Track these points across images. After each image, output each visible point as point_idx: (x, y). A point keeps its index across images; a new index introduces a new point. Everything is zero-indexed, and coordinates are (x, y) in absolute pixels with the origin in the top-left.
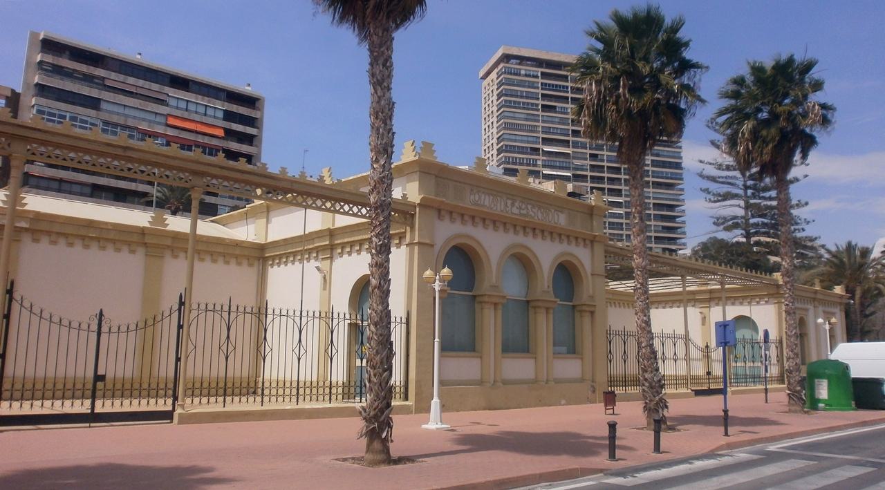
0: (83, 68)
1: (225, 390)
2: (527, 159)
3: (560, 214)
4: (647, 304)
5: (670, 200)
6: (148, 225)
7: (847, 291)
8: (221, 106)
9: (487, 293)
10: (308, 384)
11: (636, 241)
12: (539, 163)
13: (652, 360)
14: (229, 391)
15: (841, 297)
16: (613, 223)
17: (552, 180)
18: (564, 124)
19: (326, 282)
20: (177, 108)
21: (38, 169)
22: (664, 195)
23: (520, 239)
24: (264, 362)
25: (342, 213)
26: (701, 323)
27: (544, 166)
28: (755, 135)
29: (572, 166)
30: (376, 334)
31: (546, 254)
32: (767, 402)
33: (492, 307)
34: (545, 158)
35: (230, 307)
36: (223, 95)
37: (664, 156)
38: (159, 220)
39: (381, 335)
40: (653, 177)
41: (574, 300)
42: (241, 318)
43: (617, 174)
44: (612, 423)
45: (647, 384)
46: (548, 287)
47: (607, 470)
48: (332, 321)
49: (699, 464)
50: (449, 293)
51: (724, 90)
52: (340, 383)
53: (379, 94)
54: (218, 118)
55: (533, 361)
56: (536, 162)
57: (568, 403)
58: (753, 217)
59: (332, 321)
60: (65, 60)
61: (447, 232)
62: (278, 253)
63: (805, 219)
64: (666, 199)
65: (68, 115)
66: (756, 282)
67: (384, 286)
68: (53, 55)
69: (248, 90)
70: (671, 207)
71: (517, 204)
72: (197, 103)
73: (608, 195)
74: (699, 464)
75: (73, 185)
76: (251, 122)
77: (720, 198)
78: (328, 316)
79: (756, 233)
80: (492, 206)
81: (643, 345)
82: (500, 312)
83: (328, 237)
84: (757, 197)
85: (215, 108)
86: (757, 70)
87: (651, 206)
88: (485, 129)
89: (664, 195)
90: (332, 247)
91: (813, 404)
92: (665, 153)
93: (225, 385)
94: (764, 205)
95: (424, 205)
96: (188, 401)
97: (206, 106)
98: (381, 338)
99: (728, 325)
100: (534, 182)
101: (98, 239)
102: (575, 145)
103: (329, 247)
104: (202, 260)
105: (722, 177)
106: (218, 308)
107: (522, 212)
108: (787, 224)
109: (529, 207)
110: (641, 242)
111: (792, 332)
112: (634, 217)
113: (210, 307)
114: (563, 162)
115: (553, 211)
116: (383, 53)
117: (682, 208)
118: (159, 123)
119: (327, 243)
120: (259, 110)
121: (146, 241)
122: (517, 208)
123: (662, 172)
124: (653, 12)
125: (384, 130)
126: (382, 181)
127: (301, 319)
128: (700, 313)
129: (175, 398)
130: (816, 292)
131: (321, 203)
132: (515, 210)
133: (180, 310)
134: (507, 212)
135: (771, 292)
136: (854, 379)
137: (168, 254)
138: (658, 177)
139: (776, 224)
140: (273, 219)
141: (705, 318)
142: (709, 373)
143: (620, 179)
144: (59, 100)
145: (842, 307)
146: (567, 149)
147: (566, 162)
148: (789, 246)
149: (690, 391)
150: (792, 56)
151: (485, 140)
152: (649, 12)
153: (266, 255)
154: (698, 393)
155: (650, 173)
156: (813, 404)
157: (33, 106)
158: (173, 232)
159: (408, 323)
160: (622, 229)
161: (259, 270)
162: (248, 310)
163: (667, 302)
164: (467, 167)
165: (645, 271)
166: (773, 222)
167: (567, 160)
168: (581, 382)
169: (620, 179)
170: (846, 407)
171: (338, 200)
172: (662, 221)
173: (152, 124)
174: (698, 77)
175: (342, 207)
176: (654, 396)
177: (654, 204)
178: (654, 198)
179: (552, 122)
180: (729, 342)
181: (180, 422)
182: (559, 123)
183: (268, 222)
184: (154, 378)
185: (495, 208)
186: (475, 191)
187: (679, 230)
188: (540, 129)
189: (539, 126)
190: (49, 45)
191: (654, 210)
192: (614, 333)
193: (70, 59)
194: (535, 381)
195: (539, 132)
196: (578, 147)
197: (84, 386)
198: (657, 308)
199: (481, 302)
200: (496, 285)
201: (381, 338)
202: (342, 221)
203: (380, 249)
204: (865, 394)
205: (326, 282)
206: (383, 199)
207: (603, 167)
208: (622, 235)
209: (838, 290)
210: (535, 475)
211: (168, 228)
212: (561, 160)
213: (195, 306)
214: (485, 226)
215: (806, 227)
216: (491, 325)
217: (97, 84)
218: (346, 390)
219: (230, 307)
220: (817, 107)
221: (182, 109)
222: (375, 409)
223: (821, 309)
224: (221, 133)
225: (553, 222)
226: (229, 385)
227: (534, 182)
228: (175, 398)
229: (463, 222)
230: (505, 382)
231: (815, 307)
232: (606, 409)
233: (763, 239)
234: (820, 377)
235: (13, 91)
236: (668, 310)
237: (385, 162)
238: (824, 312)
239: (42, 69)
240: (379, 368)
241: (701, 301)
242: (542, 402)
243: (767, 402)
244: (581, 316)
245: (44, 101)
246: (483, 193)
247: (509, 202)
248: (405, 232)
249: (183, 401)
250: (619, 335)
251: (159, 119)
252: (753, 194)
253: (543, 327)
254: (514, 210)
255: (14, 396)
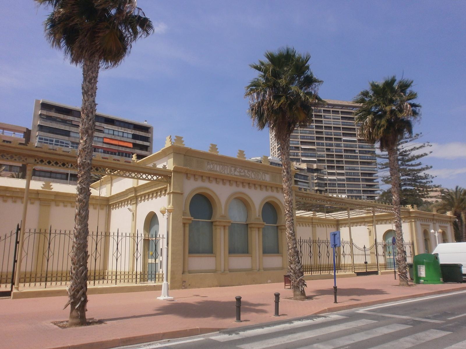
0: (62, 116)
1: (95, 277)
2: (293, 153)
3: (266, 175)
4: (292, 223)
5: (370, 170)
6: (41, 189)
7: (455, 214)
8: (131, 132)
9: (218, 220)
10: (123, 273)
11: (285, 185)
12: (300, 154)
13: (295, 257)
14: (97, 278)
15: (450, 217)
16: (340, 184)
17: (305, 163)
18: (311, 134)
19: (134, 216)
20: (109, 134)
21: (39, 167)
22: (367, 168)
23: (240, 189)
24: (137, 261)
25: (141, 179)
26: (368, 234)
27: (302, 156)
28: (373, 124)
29: (316, 155)
30: (76, 243)
31: (257, 198)
32: (395, 279)
33: (257, 230)
34: (302, 152)
35: (118, 233)
36: (132, 126)
37: (366, 148)
38: (47, 186)
39: (79, 244)
40: (360, 159)
41: (277, 223)
42: (124, 239)
43: (341, 158)
44: (238, 298)
45: (292, 271)
46: (259, 216)
47: (223, 329)
48: (137, 238)
49: (297, 324)
50: (192, 220)
51: (355, 99)
52: (139, 272)
53: (85, 99)
54: (129, 138)
55: (214, 259)
56: (298, 154)
57: (273, 282)
58: (403, 176)
59: (137, 238)
60: (52, 113)
61: (192, 186)
62: (114, 202)
63: (431, 176)
64: (368, 170)
65: (54, 140)
66: (388, 209)
67: (82, 214)
68: (47, 111)
69: (145, 123)
70: (371, 174)
71: (238, 170)
72: (119, 131)
73: (337, 170)
74: (297, 324)
75: (57, 174)
76: (146, 139)
77: (384, 166)
78: (134, 236)
79: (405, 184)
80: (222, 171)
81: (290, 248)
82: (227, 231)
83: (134, 192)
84: (404, 165)
85: (128, 133)
86: (374, 87)
87: (360, 174)
88: (271, 138)
89: (367, 168)
90: (136, 197)
91: (417, 280)
92: (366, 146)
93: (47, 275)
94: (409, 169)
95: (176, 171)
96: (21, 285)
97: (123, 132)
98: (79, 246)
99: (336, 234)
100: (296, 164)
101: (12, 197)
102: (318, 144)
103: (135, 197)
104: (32, 203)
105: (385, 155)
106: (68, 232)
107: (241, 174)
108: (395, 174)
109: (246, 171)
110: (288, 186)
111: (399, 238)
112: (284, 172)
113: (63, 232)
114: (312, 153)
115: (261, 173)
116: (89, 75)
117: (376, 175)
118: (99, 142)
119: (134, 195)
120: (150, 133)
121: (39, 197)
122: (238, 172)
123: (365, 156)
124: (290, 52)
125: (87, 120)
126: (84, 150)
127: (97, 237)
128: (368, 229)
129: (13, 284)
130: (434, 215)
131: (123, 173)
132: (236, 173)
133: (17, 233)
134: (231, 174)
135: (406, 216)
136: (441, 265)
137: (53, 204)
138: (363, 159)
139: (415, 179)
140: (114, 184)
141: (371, 231)
142: (366, 263)
143: (342, 161)
144: (49, 132)
145: (452, 224)
146: (314, 146)
147: (314, 153)
148: (396, 188)
149: (354, 273)
150: (394, 77)
151: (271, 144)
152: (288, 52)
153: (110, 203)
154: (359, 274)
155: (359, 157)
156: (417, 280)
157: (37, 136)
158: (55, 192)
159: (413, 244)
160: (345, 187)
161: (107, 211)
162: (128, 235)
163: (357, 223)
164: (260, 158)
165: (290, 203)
166: (413, 178)
167: (314, 152)
168: (282, 270)
169: (342, 161)
170: (438, 282)
171: (139, 172)
172: (366, 182)
173: (96, 143)
174: (317, 87)
175: (141, 176)
176: (297, 279)
177: (361, 173)
178: (361, 170)
179: (305, 133)
180: (337, 245)
181: (14, 298)
182: (309, 134)
183: (111, 186)
184: (44, 271)
185: (223, 172)
186: (210, 163)
187: (376, 186)
188: (299, 137)
189: (299, 135)
190: (45, 106)
191: (361, 176)
192: (321, 242)
193: (55, 112)
194: (251, 270)
195: (298, 139)
196: (319, 145)
197: (62, 274)
198: (345, 227)
199: (281, 229)
200: (225, 215)
201: (79, 246)
202: (142, 182)
203: (81, 191)
204: (450, 273)
205: (134, 216)
206: (84, 161)
207: (333, 155)
208: (345, 190)
209: (449, 214)
210: (159, 334)
211: (53, 190)
212: (311, 152)
213: (27, 230)
214: (217, 182)
215: (432, 180)
216: (222, 238)
217: (68, 123)
218: (142, 276)
219: (118, 233)
220: (409, 106)
221: (111, 134)
222: (73, 290)
223: (437, 225)
224: (131, 146)
225: (261, 179)
226: (97, 274)
227: (296, 164)
228: (13, 284)
229: (203, 180)
230: (231, 271)
231: (433, 223)
232: (285, 286)
233: (408, 187)
234: (422, 264)
235: (27, 129)
236: (358, 227)
237: (87, 139)
238: (440, 226)
239: (41, 118)
240: (77, 264)
241: (369, 222)
242: (254, 282)
243: (395, 279)
244: (282, 232)
245: (42, 133)
246: (216, 164)
247: (233, 169)
248: (167, 187)
249: (18, 285)
250: (306, 242)
251: (100, 140)
252: (402, 163)
253: (256, 240)
254: (236, 173)
255: (31, 280)
